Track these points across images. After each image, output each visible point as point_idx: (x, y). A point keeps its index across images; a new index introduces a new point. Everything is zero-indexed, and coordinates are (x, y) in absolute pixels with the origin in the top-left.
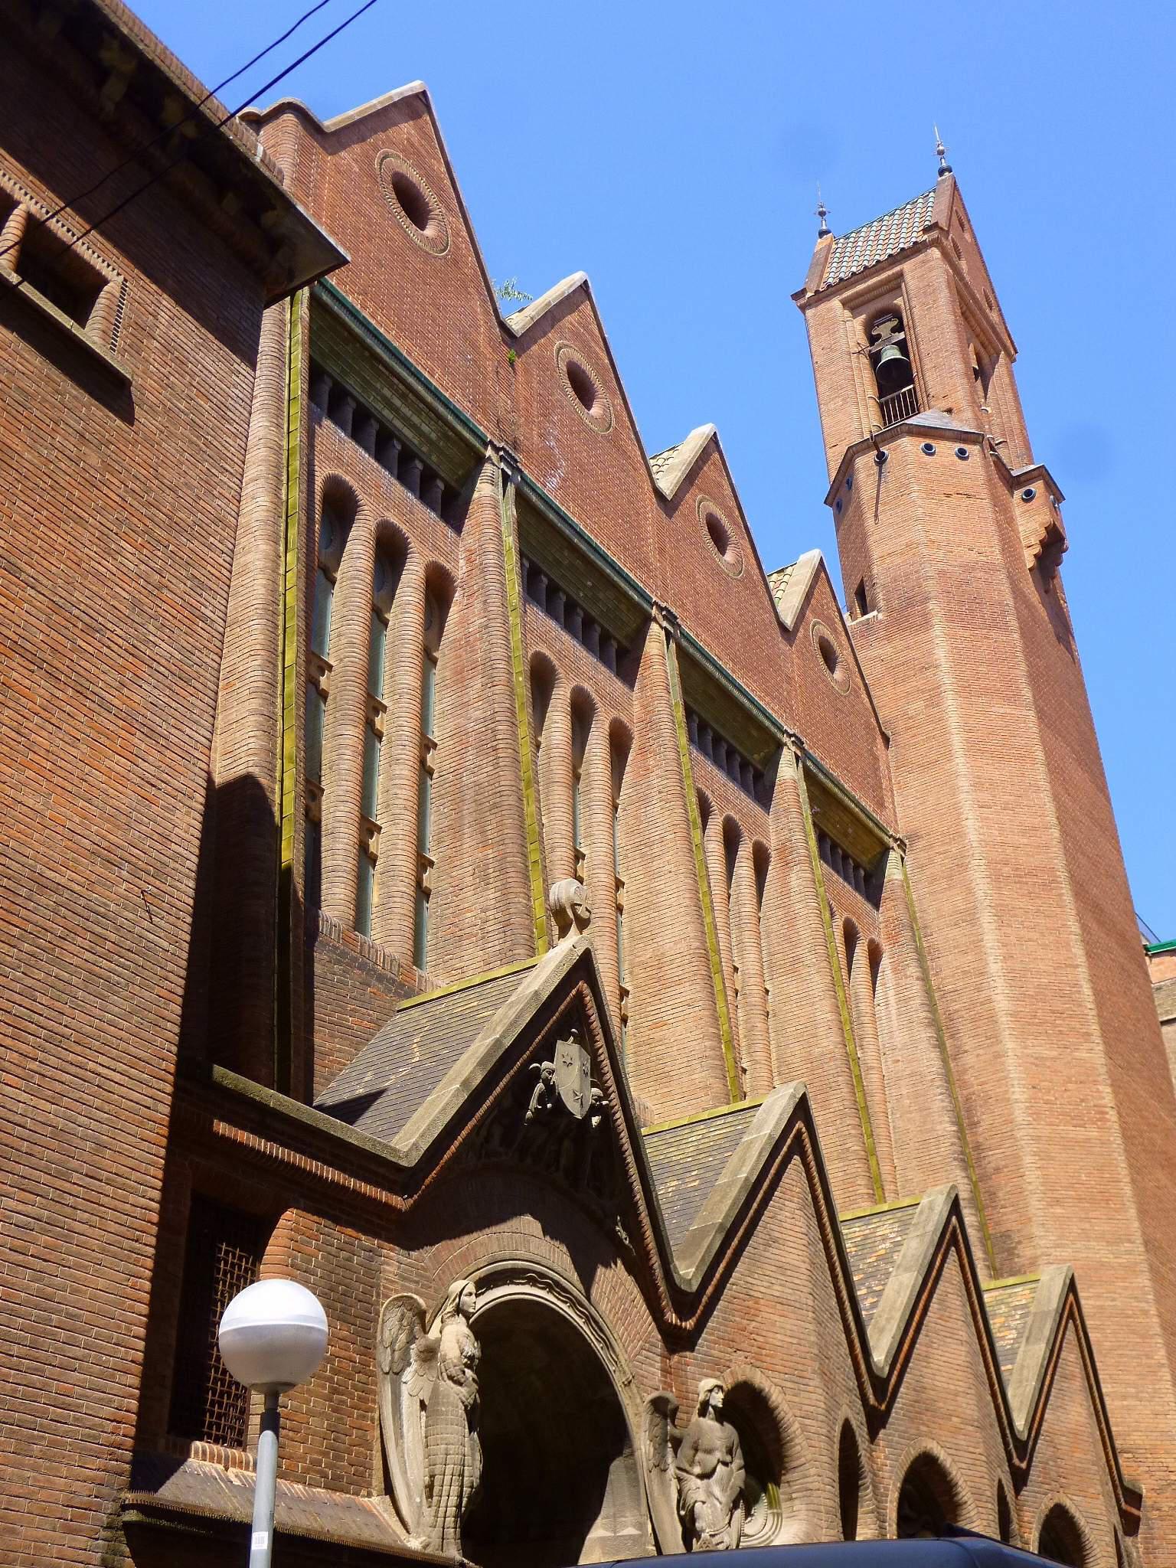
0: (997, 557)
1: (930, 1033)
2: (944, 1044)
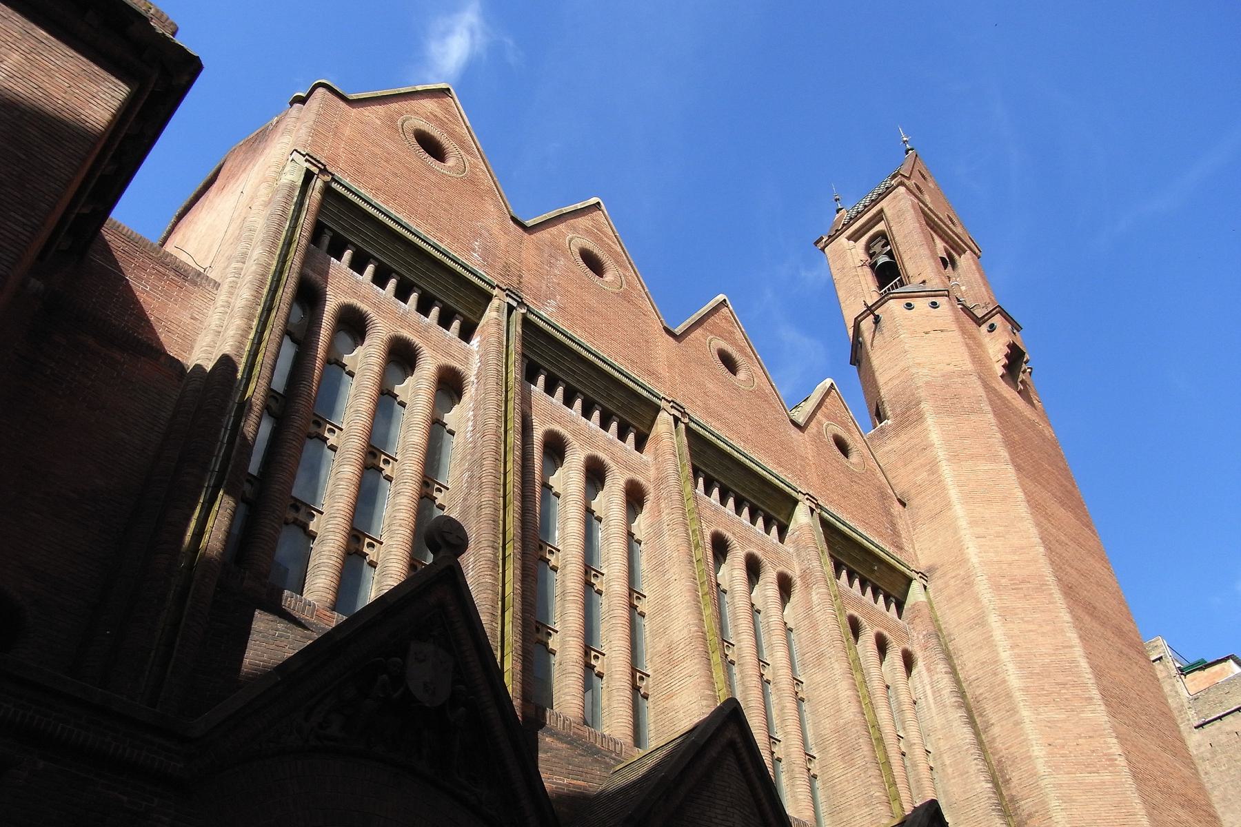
0: (969, 366)
1: (962, 712)
2: (975, 722)
